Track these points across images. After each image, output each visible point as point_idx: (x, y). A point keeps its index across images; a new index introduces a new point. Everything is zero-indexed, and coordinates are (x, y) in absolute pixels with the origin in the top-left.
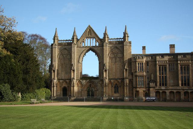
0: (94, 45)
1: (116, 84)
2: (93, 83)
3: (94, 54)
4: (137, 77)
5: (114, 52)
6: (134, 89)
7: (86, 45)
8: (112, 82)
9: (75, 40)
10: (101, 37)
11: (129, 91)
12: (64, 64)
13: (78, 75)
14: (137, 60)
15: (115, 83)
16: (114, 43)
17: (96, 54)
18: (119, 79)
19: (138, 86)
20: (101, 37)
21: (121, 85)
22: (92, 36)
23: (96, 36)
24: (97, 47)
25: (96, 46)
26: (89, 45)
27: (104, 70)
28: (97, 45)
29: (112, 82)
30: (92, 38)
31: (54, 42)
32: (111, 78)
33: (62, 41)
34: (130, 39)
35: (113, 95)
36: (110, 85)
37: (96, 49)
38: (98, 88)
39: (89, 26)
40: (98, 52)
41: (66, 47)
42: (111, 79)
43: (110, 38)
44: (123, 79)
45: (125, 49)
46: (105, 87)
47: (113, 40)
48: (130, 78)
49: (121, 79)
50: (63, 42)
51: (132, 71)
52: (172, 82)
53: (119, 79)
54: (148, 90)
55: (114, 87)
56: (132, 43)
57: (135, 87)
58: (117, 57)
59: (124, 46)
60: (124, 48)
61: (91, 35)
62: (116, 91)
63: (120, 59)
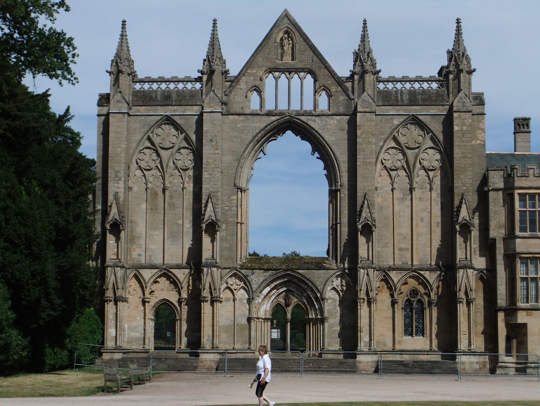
0: (308, 106)
1: (414, 292)
3: (307, 146)
4: (518, 262)
5: (402, 139)
7: (269, 106)
8: (396, 280)
9: (217, 78)
10: (343, 67)
12: (160, 194)
13: (424, 110)
14: (517, 183)
15: (406, 289)
16: (406, 97)
17: (319, 147)
19: (520, 304)
20: (343, 67)
22: (297, 64)
23: (316, 66)
26: (283, 106)
27: (204, 226)
30: (297, 71)
31: (116, 82)
32: (391, 263)
33: (154, 81)
34: (477, 84)
35: (400, 342)
37: (316, 124)
39: (286, 15)
41: (415, 110)
42: (391, 269)
43: (383, 75)
45: (456, 128)
47: (399, 86)
50: (155, 86)
52: (504, 232)
55: (401, 301)
56: (486, 98)
59: (455, 115)
60: (456, 122)
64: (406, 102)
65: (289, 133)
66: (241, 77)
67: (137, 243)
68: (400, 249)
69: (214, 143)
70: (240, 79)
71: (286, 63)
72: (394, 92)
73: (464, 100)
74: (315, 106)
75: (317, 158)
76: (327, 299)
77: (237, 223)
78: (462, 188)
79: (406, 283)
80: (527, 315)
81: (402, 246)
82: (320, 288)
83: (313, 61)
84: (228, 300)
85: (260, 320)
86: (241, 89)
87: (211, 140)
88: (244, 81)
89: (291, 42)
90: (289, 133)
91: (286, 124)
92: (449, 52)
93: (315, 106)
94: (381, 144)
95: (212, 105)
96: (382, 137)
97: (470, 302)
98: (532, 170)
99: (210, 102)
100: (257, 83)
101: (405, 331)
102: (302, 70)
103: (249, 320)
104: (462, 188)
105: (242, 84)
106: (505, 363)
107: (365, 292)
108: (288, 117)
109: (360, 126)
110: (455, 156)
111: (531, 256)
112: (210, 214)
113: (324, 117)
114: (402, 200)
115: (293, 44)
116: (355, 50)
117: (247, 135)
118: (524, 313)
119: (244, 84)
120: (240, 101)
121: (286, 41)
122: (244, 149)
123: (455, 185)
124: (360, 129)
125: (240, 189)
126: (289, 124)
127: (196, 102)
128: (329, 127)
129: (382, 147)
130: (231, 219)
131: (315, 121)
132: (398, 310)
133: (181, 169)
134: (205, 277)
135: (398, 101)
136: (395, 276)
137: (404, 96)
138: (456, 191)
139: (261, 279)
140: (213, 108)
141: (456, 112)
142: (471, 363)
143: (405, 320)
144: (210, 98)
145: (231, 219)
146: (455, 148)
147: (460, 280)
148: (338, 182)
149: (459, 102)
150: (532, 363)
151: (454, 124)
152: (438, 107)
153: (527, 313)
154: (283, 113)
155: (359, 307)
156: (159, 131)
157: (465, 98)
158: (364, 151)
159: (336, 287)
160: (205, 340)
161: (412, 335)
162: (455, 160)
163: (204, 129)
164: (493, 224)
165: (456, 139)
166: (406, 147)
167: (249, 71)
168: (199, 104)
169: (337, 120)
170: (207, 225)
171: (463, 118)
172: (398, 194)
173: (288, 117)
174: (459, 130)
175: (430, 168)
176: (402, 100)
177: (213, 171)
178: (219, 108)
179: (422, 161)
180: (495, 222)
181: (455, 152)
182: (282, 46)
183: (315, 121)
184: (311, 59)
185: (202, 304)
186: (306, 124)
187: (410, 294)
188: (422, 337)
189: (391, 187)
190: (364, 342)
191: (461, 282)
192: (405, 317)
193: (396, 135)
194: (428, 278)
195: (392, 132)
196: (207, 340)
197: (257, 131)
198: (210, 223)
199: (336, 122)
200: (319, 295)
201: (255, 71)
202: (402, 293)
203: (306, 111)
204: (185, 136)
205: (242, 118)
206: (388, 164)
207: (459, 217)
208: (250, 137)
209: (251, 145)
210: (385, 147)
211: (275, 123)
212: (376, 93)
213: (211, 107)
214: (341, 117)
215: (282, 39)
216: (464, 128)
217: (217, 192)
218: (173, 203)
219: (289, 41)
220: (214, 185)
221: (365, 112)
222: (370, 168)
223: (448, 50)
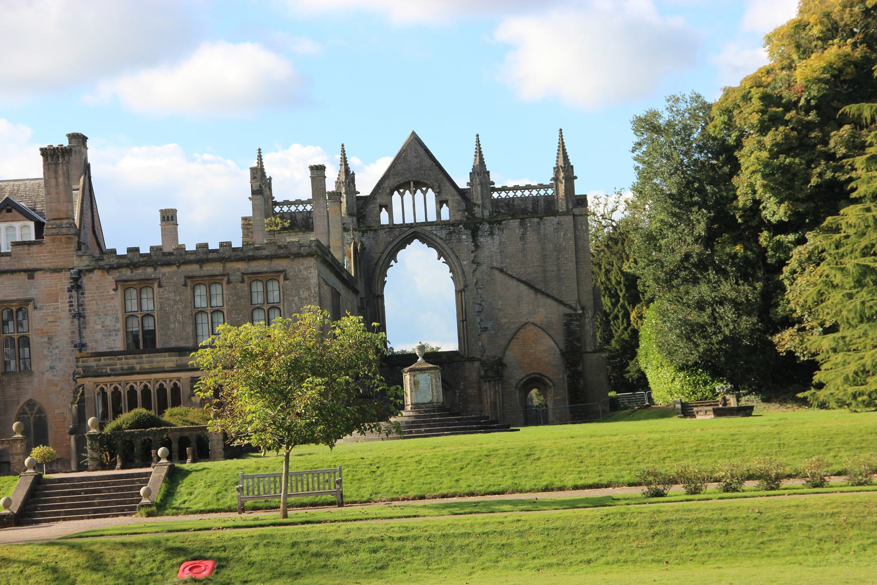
0: (432, 218)
7: (398, 220)
20: (462, 181)
25: (440, 224)
43: (498, 185)
65: (416, 241)
74: (439, 214)
90: (416, 241)
93: (439, 214)
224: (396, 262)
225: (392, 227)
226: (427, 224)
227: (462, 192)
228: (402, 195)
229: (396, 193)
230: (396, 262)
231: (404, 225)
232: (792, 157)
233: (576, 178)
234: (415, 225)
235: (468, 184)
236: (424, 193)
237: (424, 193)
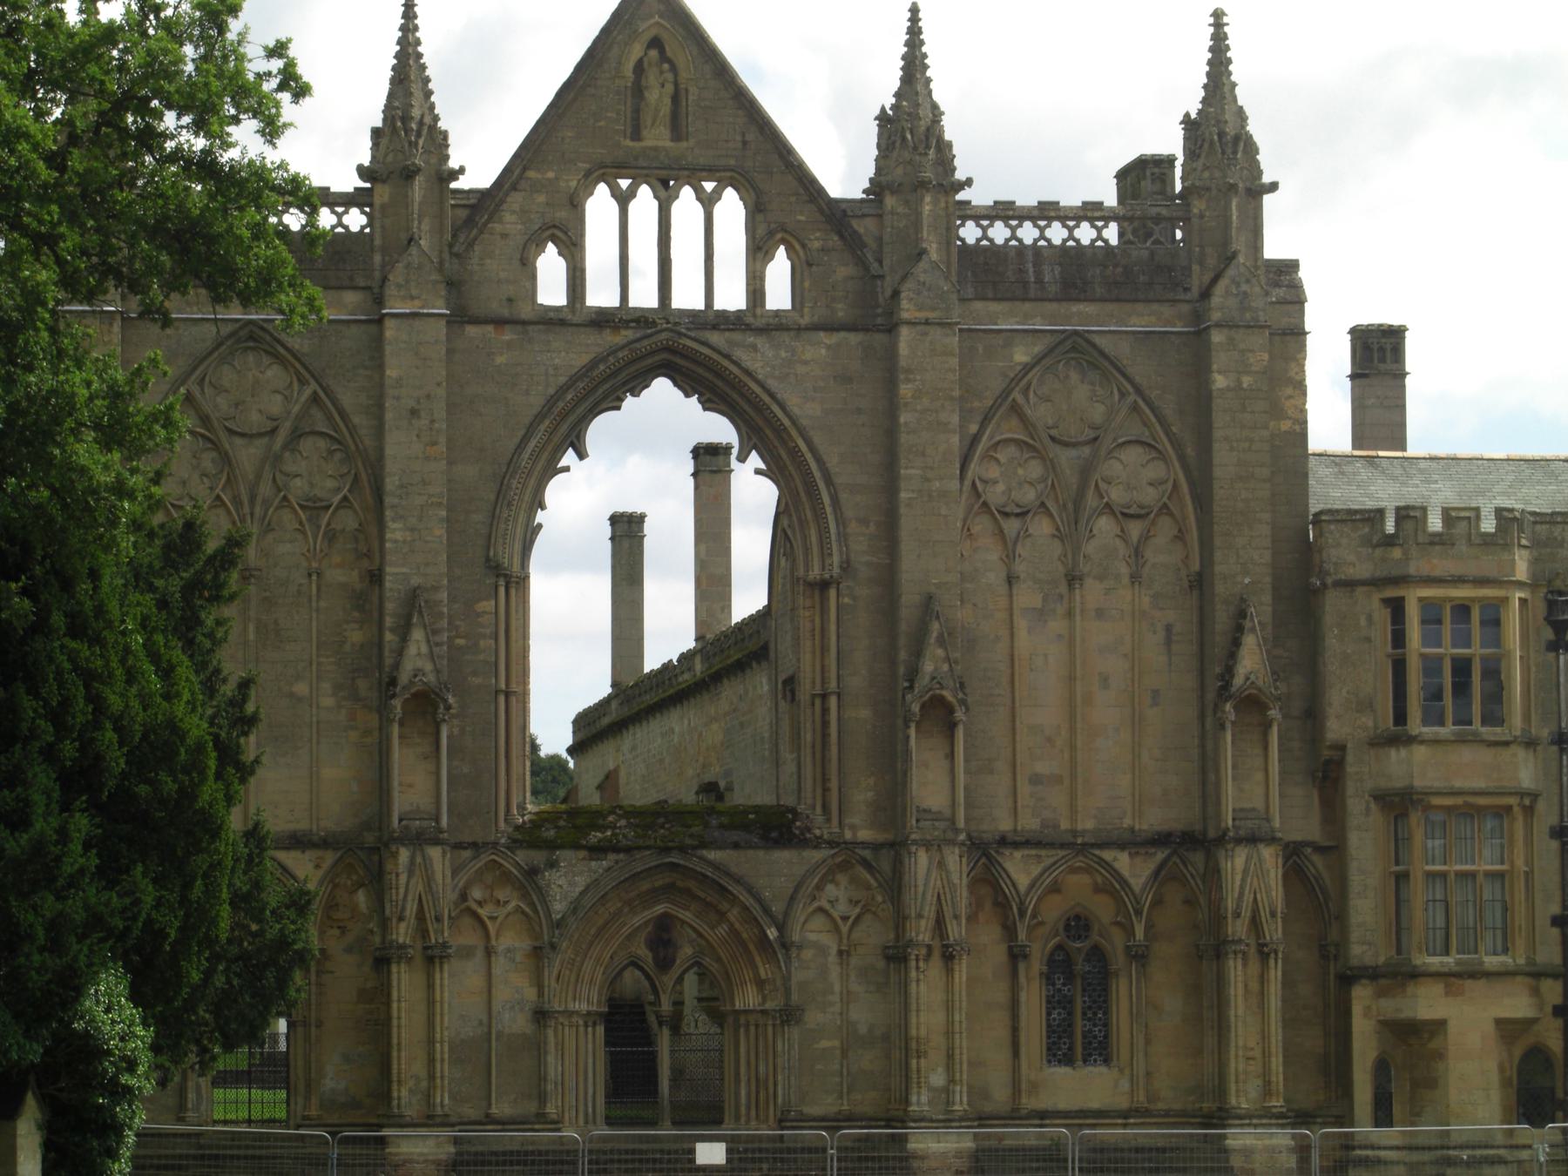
0: (731, 297)
1: (1078, 924)
2: (716, 892)
6: (1361, 995)
7: (602, 295)
8: (1023, 881)
10: (841, 164)
11: (1288, 1023)
15: (1054, 911)
16: (1051, 274)
18: (1135, 843)
20: (841, 164)
21: (1149, 927)
24: (777, 325)
25: (753, 320)
28: (779, 295)
29: (1023, 881)
32: (1005, 825)
35: (1034, 1087)
36: (989, 937)
38: (798, 976)
40: (803, 404)
41: (1085, 317)
43: (980, 196)
44: (1192, 847)
45: (1220, 381)
46: (1254, 967)
47: (1028, 233)
48: (1305, 826)
49: (1160, 840)
51: (1336, 728)
53: (1135, 843)
54: (1558, 1011)
57: (1372, 974)
58: (1091, 500)
59: (1217, 337)
60: (1219, 360)
61: (677, 132)
62: (1078, 1035)
63: (1135, 529)
64: (1053, 289)
65: (662, 387)
66: (507, 195)
67: (1127, 822)
68: (1036, 780)
69: (424, 422)
70: (502, 202)
71: (656, 149)
72: (1012, 254)
73: (1244, 287)
74: (756, 291)
75: (758, 472)
76: (800, 947)
77: (497, 692)
78: (1239, 579)
79: (1055, 888)
80: (1447, 994)
81: (1042, 768)
82: (777, 908)
83: (745, 143)
84: (467, 952)
85: (575, 1019)
86: (504, 236)
87: (414, 413)
88: (516, 207)
89: (670, 76)
90: (662, 387)
91: (657, 358)
92: (1187, 122)
93: (756, 291)
94: (974, 428)
95: (414, 292)
96: (976, 404)
97: (1268, 955)
98: (1465, 523)
99: (407, 282)
100: (558, 215)
101: (1049, 1049)
102: (710, 172)
103: (541, 1016)
104: (1239, 579)
105: (508, 217)
106: (1373, 1148)
107: (932, 923)
108: (664, 335)
109: (908, 371)
110: (1218, 472)
111: (1459, 801)
112: (419, 663)
113: (785, 337)
114: (1041, 614)
115: (676, 84)
116: (883, 109)
117: (527, 393)
118: (1437, 988)
119: (513, 218)
120: (503, 275)
121: (652, 78)
122: (517, 440)
123: (1218, 569)
124: (908, 381)
125: (506, 576)
126: (665, 356)
127: (351, 278)
128: (801, 369)
129: (975, 439)
130: (477, 681)
131: (754, 348)
132: (1028, 980)
133: (301, 506)
134: (403, 878)
135: (1025, 284)
136: (1020, 870)
137: (1046, 269)
138: (1220, 588)
139: (581, 881)
140: (416, 302)
141: (1218, 325)
142: (1272, 1150)
143: (1049, 1014)
144: (408, 266)
145: (477, 681)
146: (1216, 446)
147: (1238, 883)
148: (831, 555)
149: (1228, 293)
150: (1461, 1147)
151: (1215, 367)
152: (1155, 307)
153: (1446, 986)
154: (646, 319)
155: (913, 974)
156: (227, 376)
157: (1248, 281)
158: (924, 454)
159: (827, 906)
160: (404, 1093)
161: (1068, 1060)
162: (1216, 485)
163: (388, 372)
164: (1336, 698)
165: (1220, 420)
166: (1053, 439)
167: (531, 174)
168: (362, 284)
169: (829, 347)
170: (406, 701)
171: (1242, 346)
172: (1027, 597)
173: (664, 335)
174: (1228, 389)
175: (1131, 511)
176: (1039, 281)
177: (420, 519)
178: (441, 302)
179: (1102, 485)
180: (1344, 692)
181: (1216, 461)
182: (638, 90)
183: (754, 348)
184: (739, 138)
185: (394, 968)
186: (727, 357)
187: (1067, 927)
188: (1103, 1069)
189: (1003, 575)
190: (931, 1089)
191: (1242, 887)
192: (1048, 1002)
193: (1020, 399)
194: (1126, 873)
195: (1006, 393)
196: (411, 1091)
197: (562, 380)
198: (415, 695)
199: (823, 351)
200: (772, 933)
201: (551, 175)
202: (1041, 923)
203: (723, 314)
204: (315, 392)
205: (508, 335)
206: (995, 494)
207: (1232, 676)
208: (537, 401)
209: (542, 427)
210: (985, 438)
211: (620, 355)
212: (955, 258)
213: (412, 298)
214: (843, 334)
215: (639, 68)
216: (1246, 381)
217: (435, 589)
218: (276, 622)
219: (662, 72)
220: (427, 565)
221: (927, 323)
222: (943, 512)
223: (1187, 115)
224: (582, 455)
225: (575, 318)
226: (710, 320)
227: (836, 214)
228: (623, 200)
229: (602, 189)
230: (582, 455)
231: (619, 319)
232: (173, 269)
233: (1195, 212)
234: (665, 314)
235: (362, 172)
236: (708, 203)
237: (708, 203)
